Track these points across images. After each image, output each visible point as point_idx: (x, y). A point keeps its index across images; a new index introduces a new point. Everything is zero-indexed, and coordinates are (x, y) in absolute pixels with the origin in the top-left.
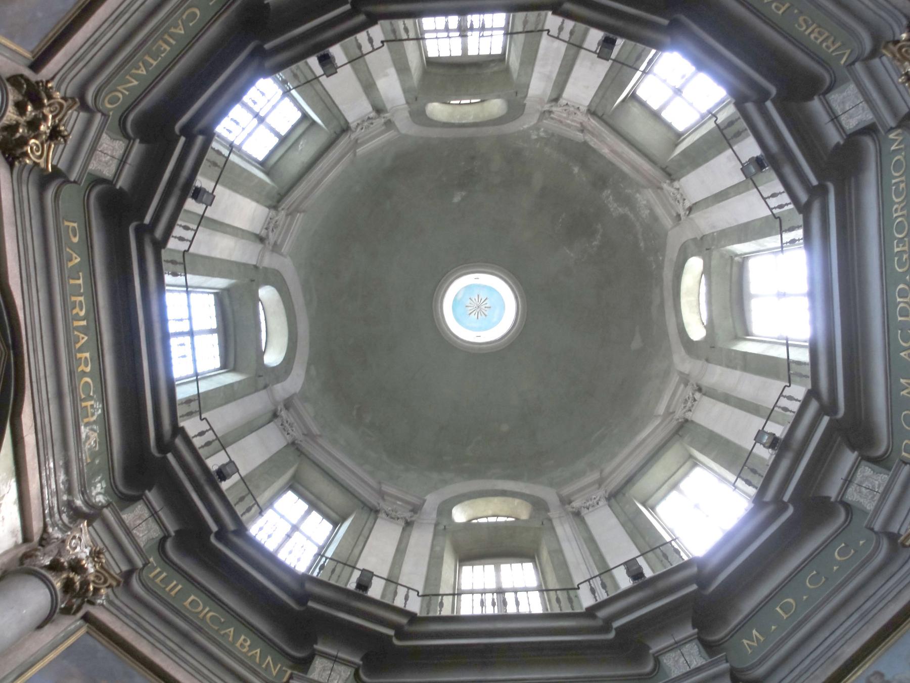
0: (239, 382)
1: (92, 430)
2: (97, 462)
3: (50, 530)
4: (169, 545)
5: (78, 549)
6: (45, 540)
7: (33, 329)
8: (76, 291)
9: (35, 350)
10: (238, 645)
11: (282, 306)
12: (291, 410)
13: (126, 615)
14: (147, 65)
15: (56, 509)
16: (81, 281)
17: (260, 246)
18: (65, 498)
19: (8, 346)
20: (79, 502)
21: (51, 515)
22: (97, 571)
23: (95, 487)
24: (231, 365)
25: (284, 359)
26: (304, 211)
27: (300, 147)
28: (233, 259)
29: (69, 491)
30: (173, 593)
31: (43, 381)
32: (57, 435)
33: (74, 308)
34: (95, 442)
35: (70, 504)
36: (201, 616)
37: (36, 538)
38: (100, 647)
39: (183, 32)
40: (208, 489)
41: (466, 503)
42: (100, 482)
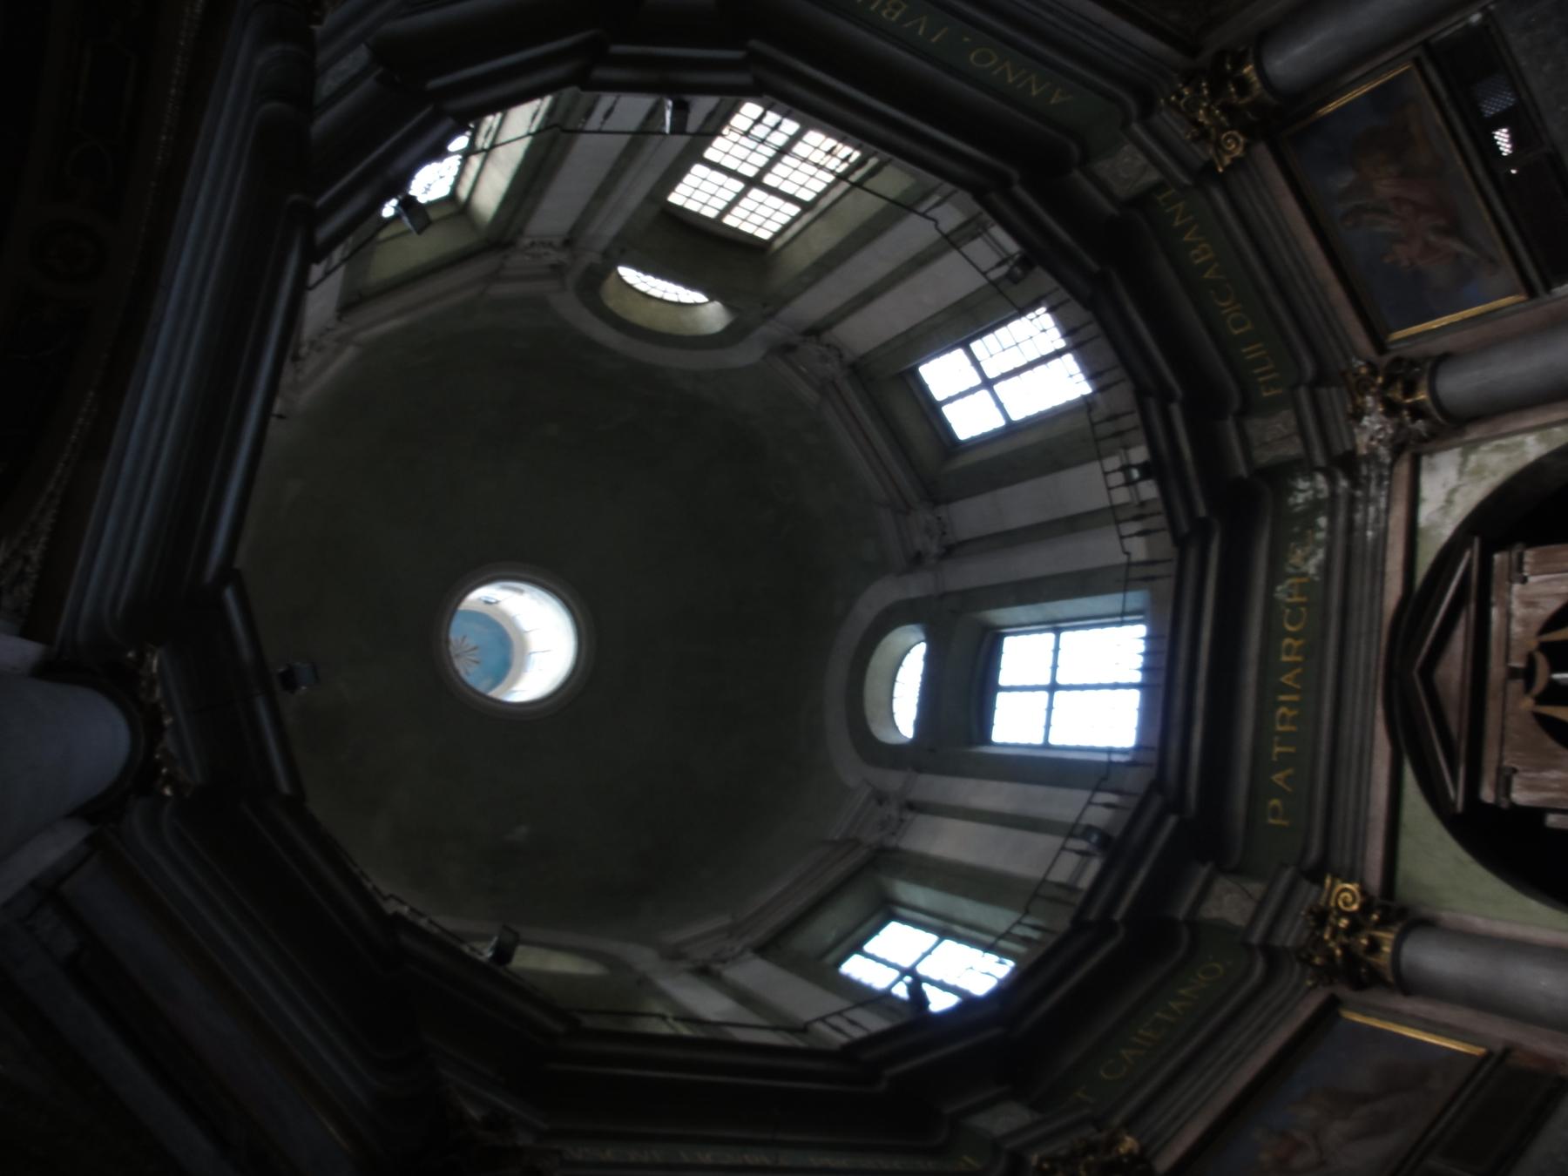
1: (1296, 568)
2: (1296, 529)
3: (1388, 460)
4: (1236, 404)
5: (1378, 427)
6: (1397, 450)
8: (1286, 738)
10: (1210, 255)
16: (1277, 749)
18: (1359, 493)
20: (1344, 483)
29: (1352, 501)
35: (1355, 483)
37: (1406, 456)
41: (687, 333)
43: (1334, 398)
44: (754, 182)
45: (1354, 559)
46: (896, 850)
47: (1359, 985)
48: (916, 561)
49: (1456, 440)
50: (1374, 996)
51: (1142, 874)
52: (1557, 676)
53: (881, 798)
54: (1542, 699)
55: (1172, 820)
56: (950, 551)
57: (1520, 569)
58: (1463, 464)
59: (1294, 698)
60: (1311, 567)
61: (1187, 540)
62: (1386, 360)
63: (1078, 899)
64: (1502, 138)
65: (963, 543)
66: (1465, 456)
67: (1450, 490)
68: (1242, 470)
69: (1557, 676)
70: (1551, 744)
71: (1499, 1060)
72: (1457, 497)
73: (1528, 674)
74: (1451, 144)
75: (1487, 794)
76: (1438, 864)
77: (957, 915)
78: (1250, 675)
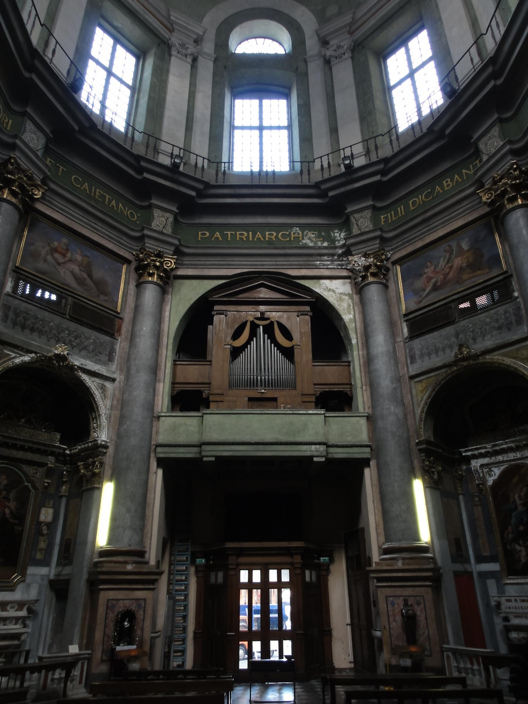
0: (297, 86)
2: (323, 234)
3: (349, 268)
4: (379, 205)
5: (360, 264)
6: (352, 270)
7: (252, 265)
8: (234, 236)
9: (263, 265)
11: (245, 24)
12: (328, 39)
13: (401, 245)
14: (110, 201)
15: (340, 263)
17: (200, 58)
19: (259, 277)
20: (340, 251)
21: (342, 265)
22: (373, 257)
23: (336, 237)
24: (286, 91)
25: (288, 29)
26: (168, 10)
27: (120, 26)
28: (210, 93)
29: (333, 255)
30: (403, 214)
31: (278, 263)
32: (305, 259)
33: (242, 238)
34: (313, 234)
35: (339, 256)
36: (421, 203)
37: (350, 274)
38: (409, 263)
39: (86, 184)
40: (355, 176)
42: (334, 233)
43: (375, 245)
44: (110, 73)
45: (309, 256)
46: (170, 55)
47: (137, 269)
48: (324, 42)
49: (354, 291)
50: (134, 276)
51: (167, 184)
52: (261, 327)
53: (198, 41)
54: (252, 323)
55: (193, 194)
56: (327, 62)
57: (301, 315)
58: (345, 294)
59: (251, 239)
60: (306, 241)
61: (319, 188)
62: (389, 265)
63: (150, 157)
64: (466, 305)
65: (331, 69)
66: (348, 295)
67: (335, 291)
68: (349, 210)
69: (261, 327)
70: (236, 326)
71: (118, 317)
72: (331, 293)
73: (262, 318)
74: (468, 287)
75: (216, 308)
76: (186, 295)
77: (141, 95)
78: (260, 220)
